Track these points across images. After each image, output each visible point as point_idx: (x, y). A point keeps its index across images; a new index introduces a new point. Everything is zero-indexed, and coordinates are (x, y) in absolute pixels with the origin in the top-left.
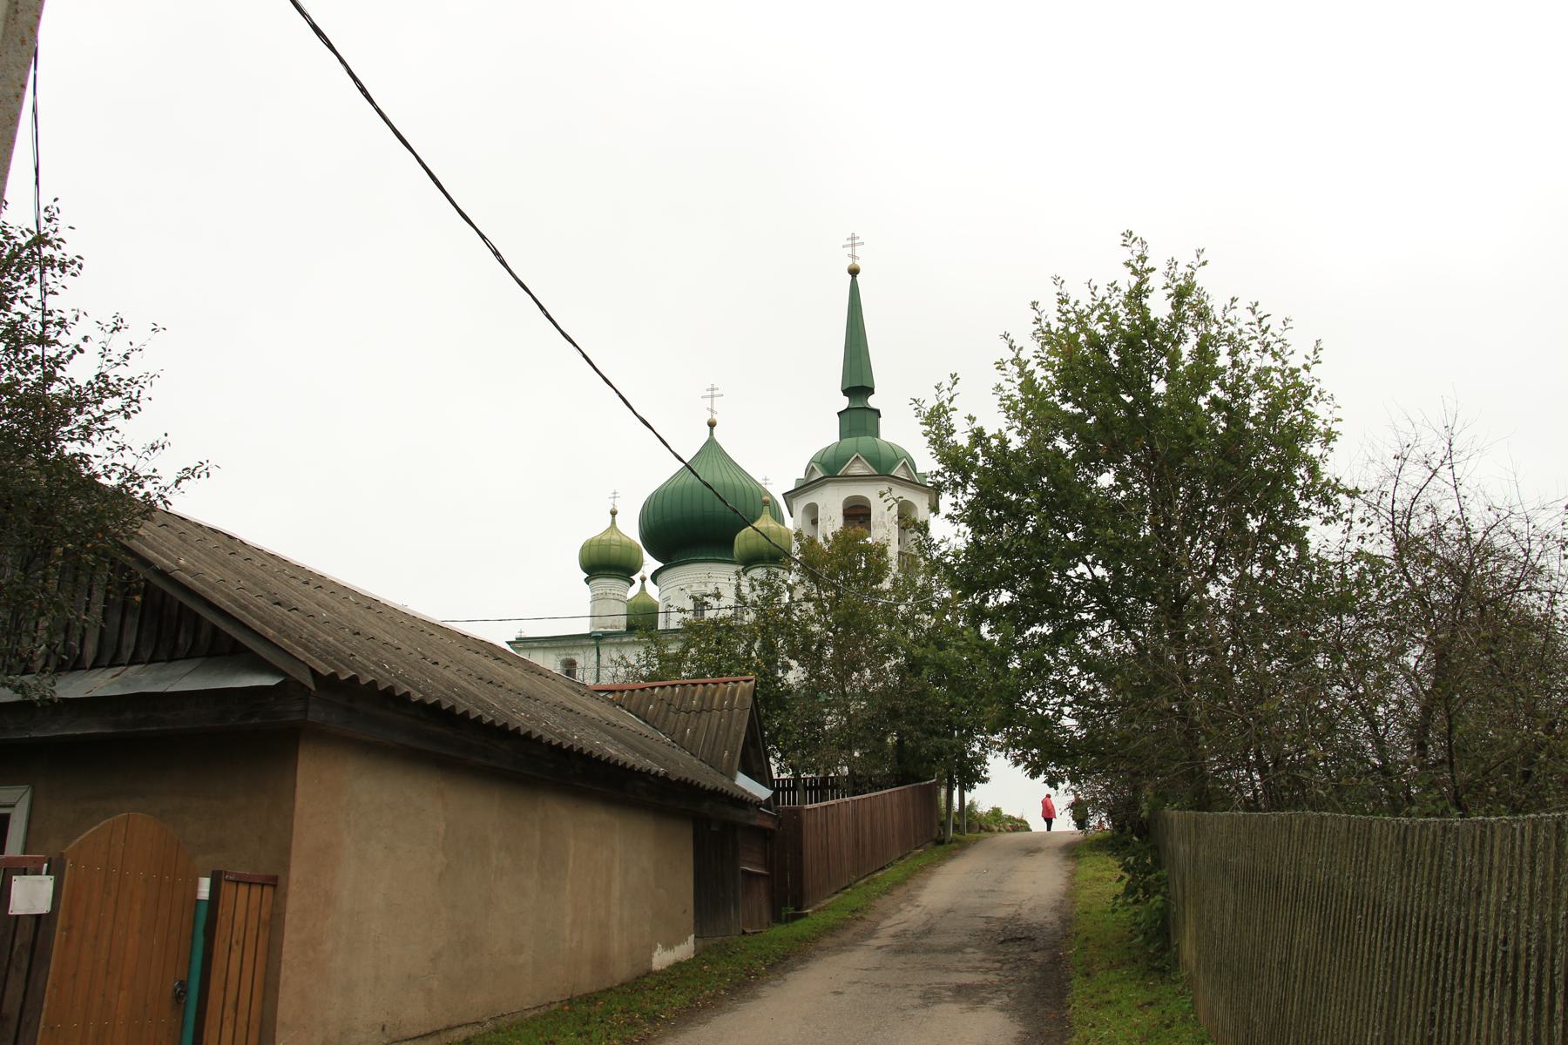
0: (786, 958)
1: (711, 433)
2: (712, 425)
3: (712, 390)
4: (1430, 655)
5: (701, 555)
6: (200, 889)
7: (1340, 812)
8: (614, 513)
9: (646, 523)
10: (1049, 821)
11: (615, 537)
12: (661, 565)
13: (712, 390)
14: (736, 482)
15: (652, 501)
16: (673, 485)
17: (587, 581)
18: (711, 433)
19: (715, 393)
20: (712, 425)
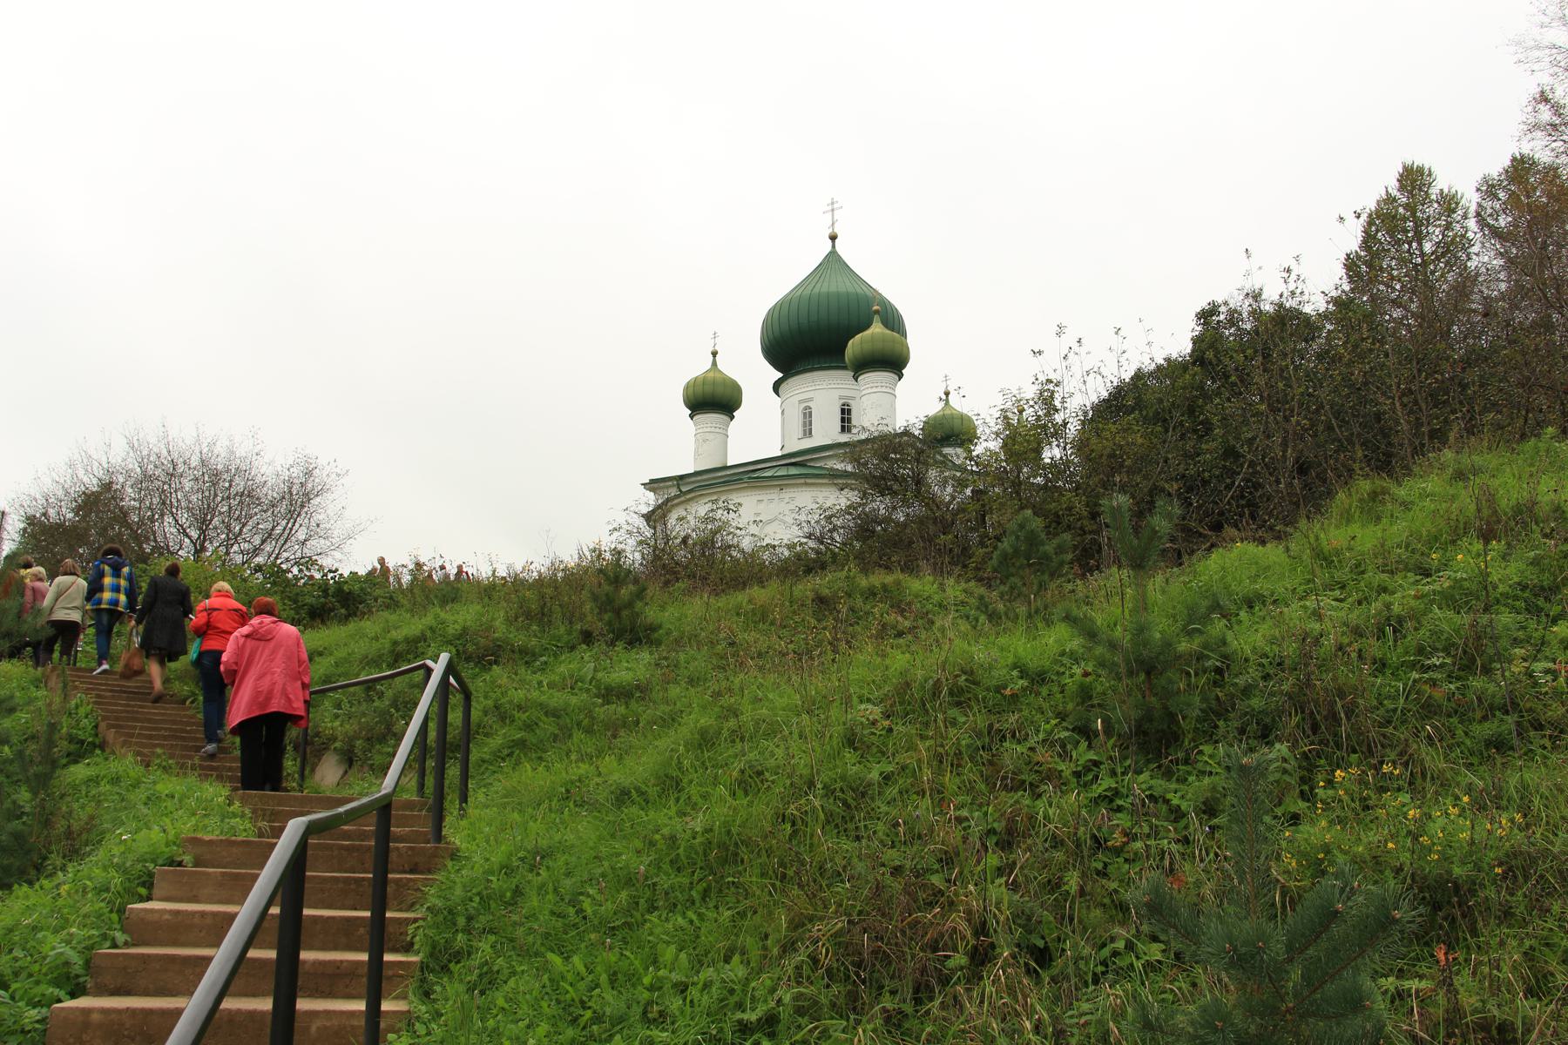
0: (521, 652)
1: (834, 246)
2: (833, 238)
3: (833, 203)
4: (459, 632)
5: (825, 363)
6: (307, 1000)
7: (1309, 750)
8: (714, 354)
9: (770, 332)
10: (1144, 697)
11: (718, 375)
12: (780, 375)
13: (833, 203)
14: (859, 291)
15: (776, 313)
16: (808, 292)
17: (691, 417)
18: (834, 246)
19: (835, 206)
20: (833, 238)
